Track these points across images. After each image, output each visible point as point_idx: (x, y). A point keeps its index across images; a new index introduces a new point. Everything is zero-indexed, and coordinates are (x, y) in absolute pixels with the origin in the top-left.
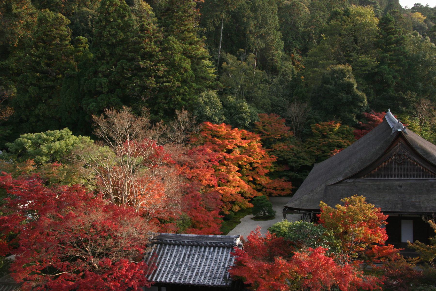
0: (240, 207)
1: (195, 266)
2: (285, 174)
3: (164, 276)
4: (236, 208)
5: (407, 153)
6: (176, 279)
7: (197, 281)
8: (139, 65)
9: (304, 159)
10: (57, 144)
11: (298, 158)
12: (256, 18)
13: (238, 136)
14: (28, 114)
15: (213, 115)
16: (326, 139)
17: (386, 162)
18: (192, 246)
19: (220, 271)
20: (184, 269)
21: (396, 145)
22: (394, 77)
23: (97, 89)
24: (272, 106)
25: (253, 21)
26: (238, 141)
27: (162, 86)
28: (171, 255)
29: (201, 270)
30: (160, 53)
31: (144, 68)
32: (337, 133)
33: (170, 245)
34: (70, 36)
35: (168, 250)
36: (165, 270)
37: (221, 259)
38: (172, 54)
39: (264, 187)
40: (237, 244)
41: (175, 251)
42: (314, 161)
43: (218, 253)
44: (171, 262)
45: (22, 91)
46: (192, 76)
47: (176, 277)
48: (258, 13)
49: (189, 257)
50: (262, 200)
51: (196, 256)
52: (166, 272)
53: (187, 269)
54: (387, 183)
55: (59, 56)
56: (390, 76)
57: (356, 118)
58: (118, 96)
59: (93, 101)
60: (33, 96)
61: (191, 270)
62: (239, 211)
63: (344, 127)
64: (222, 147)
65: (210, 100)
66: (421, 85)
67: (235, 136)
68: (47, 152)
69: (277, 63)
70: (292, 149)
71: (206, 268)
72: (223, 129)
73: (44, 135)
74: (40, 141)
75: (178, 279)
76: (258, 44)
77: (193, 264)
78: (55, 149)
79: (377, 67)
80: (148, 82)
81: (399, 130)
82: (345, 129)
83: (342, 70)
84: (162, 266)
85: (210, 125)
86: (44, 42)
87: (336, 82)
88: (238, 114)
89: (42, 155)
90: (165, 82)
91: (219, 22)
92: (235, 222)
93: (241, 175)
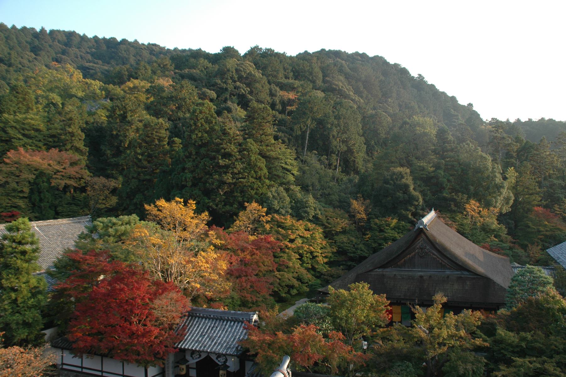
0: (298, 291)
1: (216, 336)
2: (344, 263)
3: (189, 344)
4: (294, 292)
5: (428, 247)
6: (197, 347)
7: (214, 350)
8: (218, 163)
9: (362, 250)
10: (123, 228)
11: (357, 249)
12: (339, 125)
13: (302, 228)
14: (129, 203)
15: (280, 207)
16: (382, 233)
17: (410, 254)
18: (217, 320)
19: (235, 342)
20: (206, 339)
21: (419, 240)
22: (449, 181)
23: (183, 183)
24: (340, 201)
25: (336, 127)
26: (301, 231)
27: (237, 181)
28: (198, 327)
29: (219, 341)
30: (238, 153)
31: (223, 166)
32: (393, 229)
33: (199, 317)
34: (167, 138)
35: (197, 322)
36: (191, 339)
37: (238, 332)
38: (249, 154)
39: (322, 274)
40: (253, 320)
41: (202, 323)
42: (371, 252)
43: (237, 327)
44: (197, 332)
45: (126, 183)
46: (265, 174)
47: (198, 345)
48: (341, 121)
49: (212, 329)
50: (315, 285)
51: (218, 328)
52: (191, 341)
53: (208, 339)
54: (410, 273)
55: (157, 154)
56: (445, 180)
57: (411, 215)
58: (200, 189)
59: (179, 193)
60: (133, 188)
61: (211, 340)
62: (296, 295)
63: (400, 223)
64: (285, 236)
65: (278, 194)
66: (472, 188)
67: (298, 227)
68: (114, 233)
69: (359, 164)
70: (352, 241)
71: (225, 339)
72: (289, 221)
73: (114, 220)
74: (110, 225)
75: (199, 347)
76: (340, 146)
77: (214, 335)
78: (121, 232)
79: (433, 172)
80: (225, 178)
81: (421, 227)
82: (401, 224)
83: (401, 172)
84: (189, 335)
85: (276, 217)
86: (146, 142)
87: (395, 183)
88: (303, 208)
89: (109, 236)
90: (240, 178)
91: (306, 127)
92: (289, 304)
93: (301, 263)
